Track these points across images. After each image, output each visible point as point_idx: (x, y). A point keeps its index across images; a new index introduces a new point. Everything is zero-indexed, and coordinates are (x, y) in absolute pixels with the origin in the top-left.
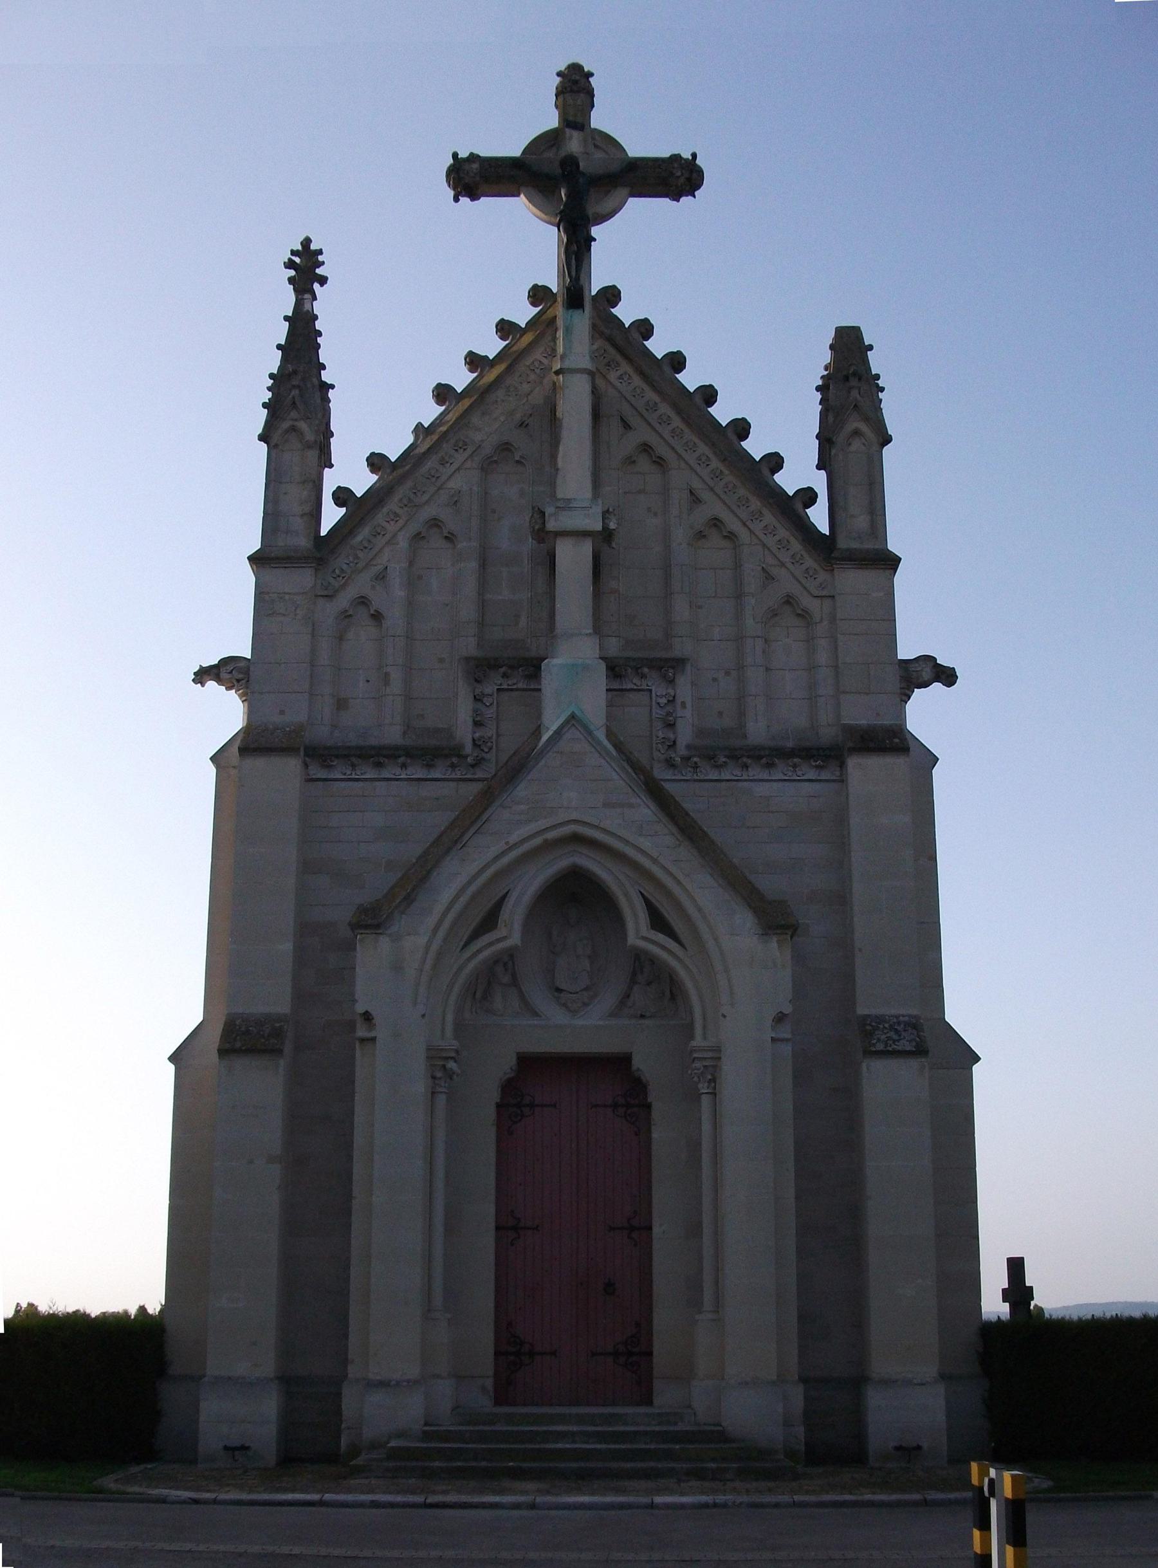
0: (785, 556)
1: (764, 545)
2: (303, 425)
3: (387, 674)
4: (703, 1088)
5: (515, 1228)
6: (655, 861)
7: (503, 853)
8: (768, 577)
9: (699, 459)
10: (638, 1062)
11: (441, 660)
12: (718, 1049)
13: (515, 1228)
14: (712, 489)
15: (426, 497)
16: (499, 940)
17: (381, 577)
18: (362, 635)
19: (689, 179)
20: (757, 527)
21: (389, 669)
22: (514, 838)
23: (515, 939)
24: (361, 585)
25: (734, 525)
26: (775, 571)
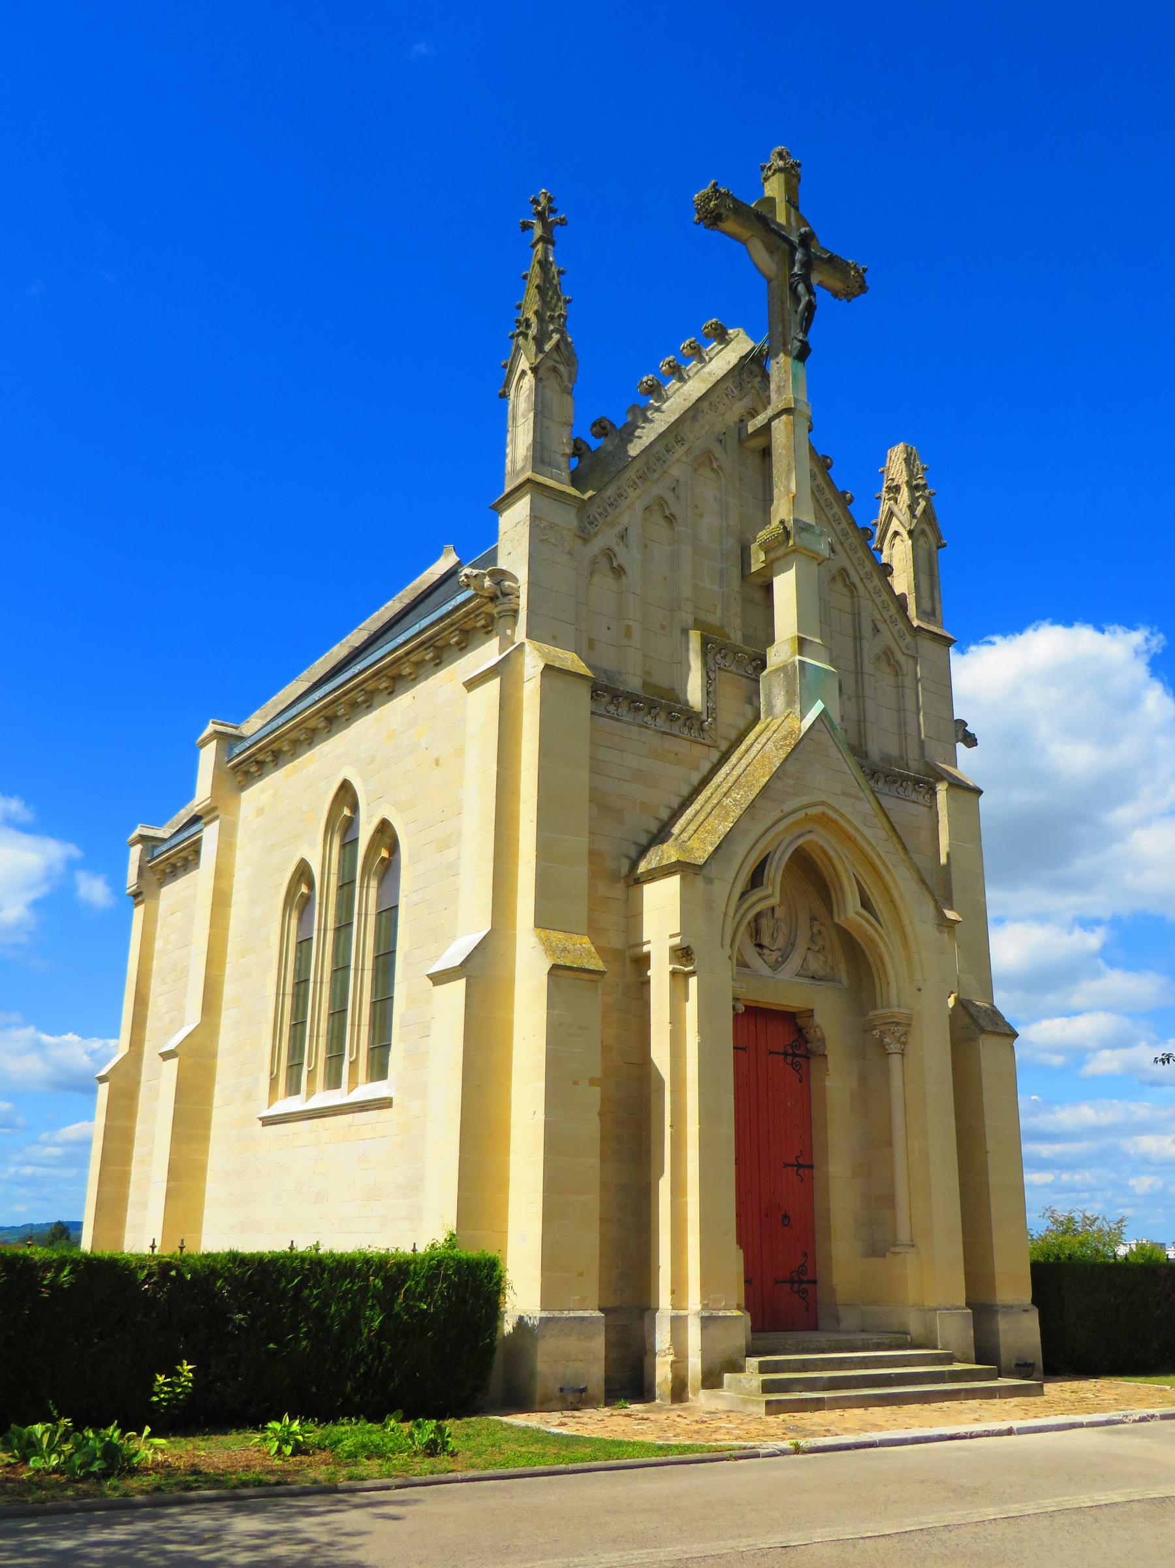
0: (886, 615)
1: (873, 601)
2: (561, 368)
3: (628, 627)
4: (894, 1048)
5: (800, 1166)
6: (874, 848)
7: (779, 820)
8: (876, 630)
9: (834, 515)
10: (819, 1018)
11: (663, 627)
12: (910, 1017)
13: (800, 1166)
14: (842, 544)
15: (656, 476)
16: (766, 897)
17: (622, 537)
18: (605, 582)
19: (860, 287)
20: (870, 586)
21: (631, 623)
22: (787, 808)
23: (775, 901)
24: (606, 538)
25: (855, 578)
26: (881, 626)
